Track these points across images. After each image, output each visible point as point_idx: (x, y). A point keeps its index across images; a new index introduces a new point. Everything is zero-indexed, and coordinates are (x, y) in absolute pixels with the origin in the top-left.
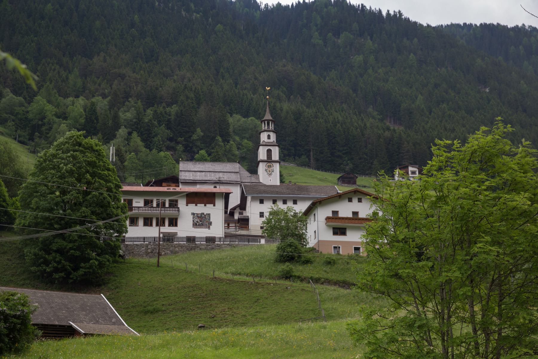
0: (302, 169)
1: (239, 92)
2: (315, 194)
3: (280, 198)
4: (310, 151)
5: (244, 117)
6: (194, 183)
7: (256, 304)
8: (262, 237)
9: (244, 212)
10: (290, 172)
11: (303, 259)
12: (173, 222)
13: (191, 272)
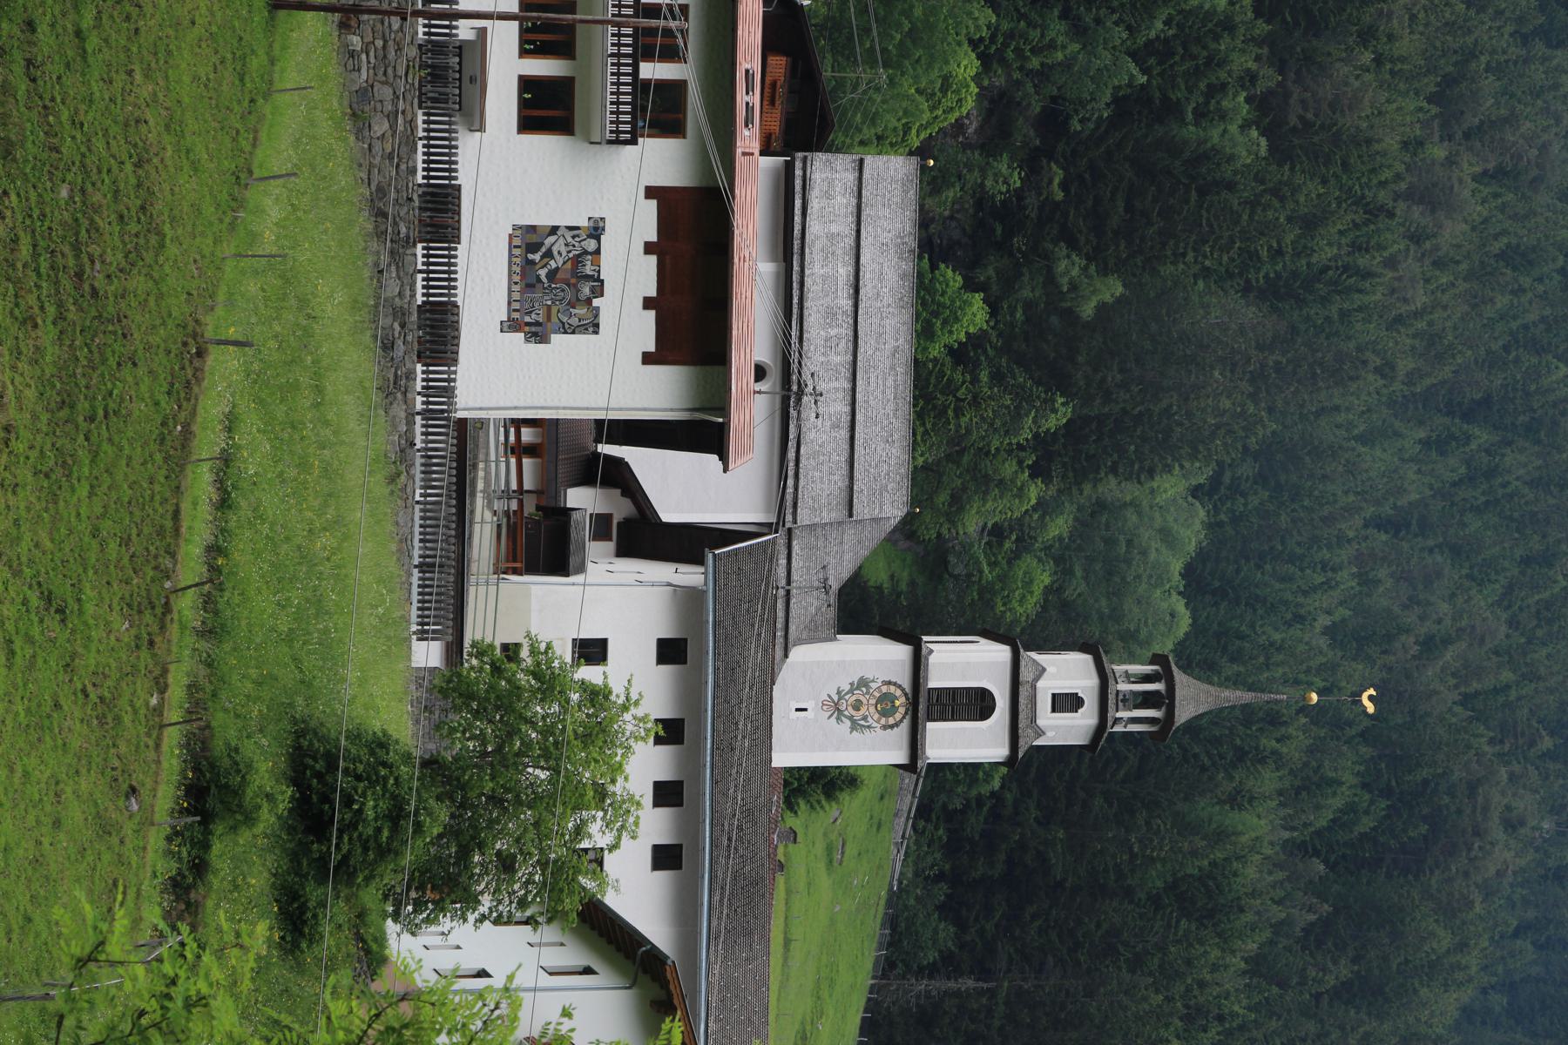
0: (873, 923)
1: (1342, 540)
2: (715, 980)
3: (691, 762)
4: (983, 972)
5: (1188, 572)
6: (788, 244)
7: (35, 601)
8: (454, 651)
9: (610, 546)
10: (851, 850)
11: (313, 893)
12: (546, 109)
13: (237, 203)
